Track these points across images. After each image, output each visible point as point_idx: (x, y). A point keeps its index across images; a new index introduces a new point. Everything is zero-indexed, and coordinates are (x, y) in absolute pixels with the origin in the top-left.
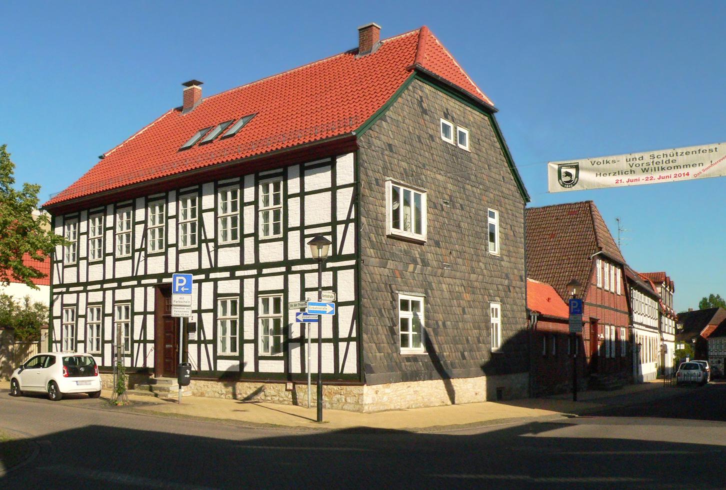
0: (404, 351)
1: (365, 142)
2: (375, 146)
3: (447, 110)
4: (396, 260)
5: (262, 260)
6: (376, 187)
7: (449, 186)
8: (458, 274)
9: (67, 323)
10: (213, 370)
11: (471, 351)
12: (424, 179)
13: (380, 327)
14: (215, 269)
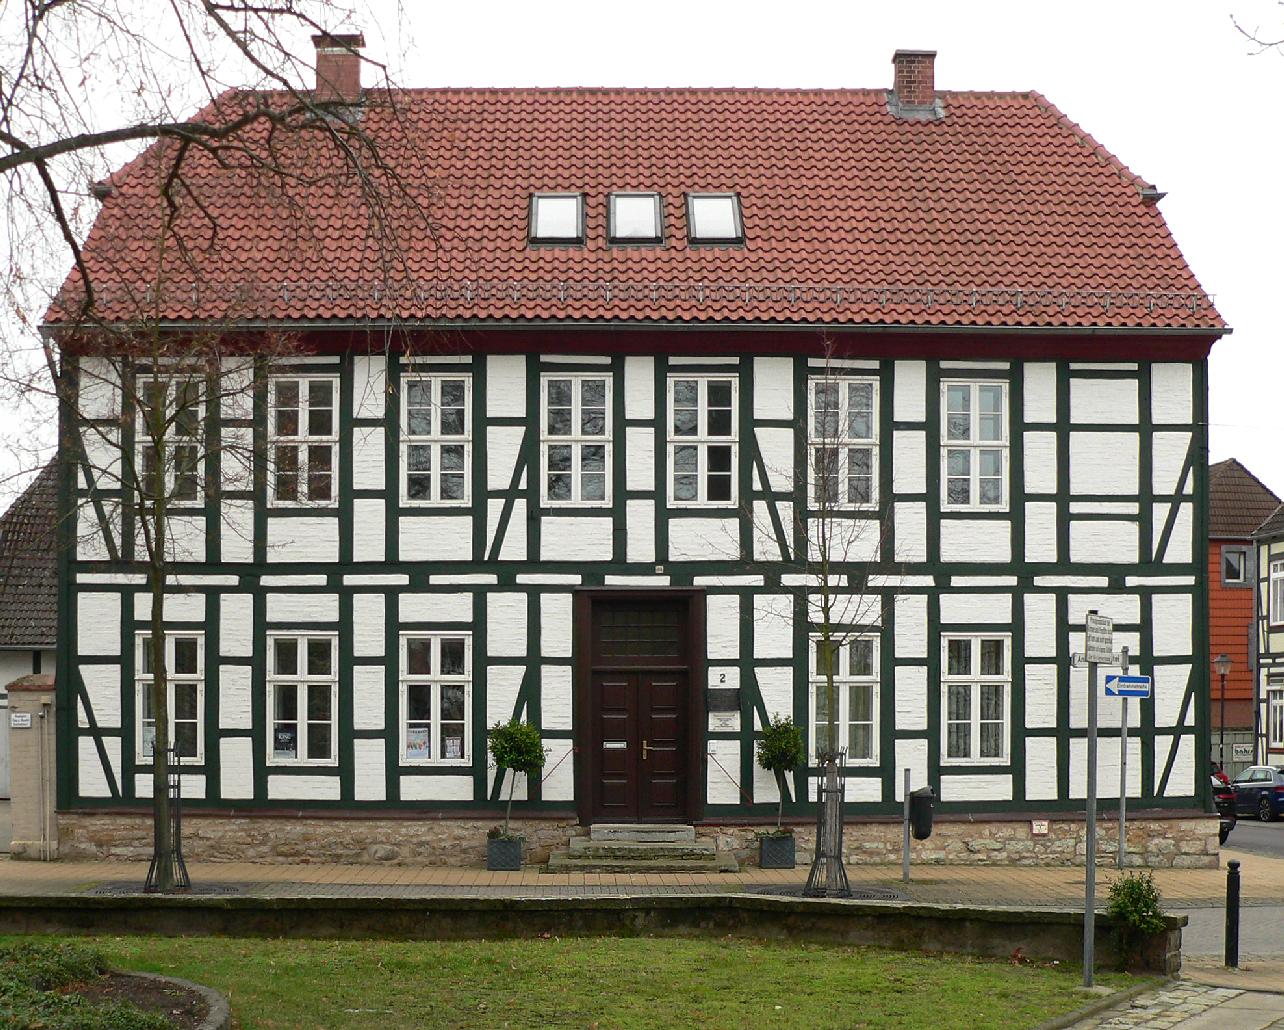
5: (948, 555)
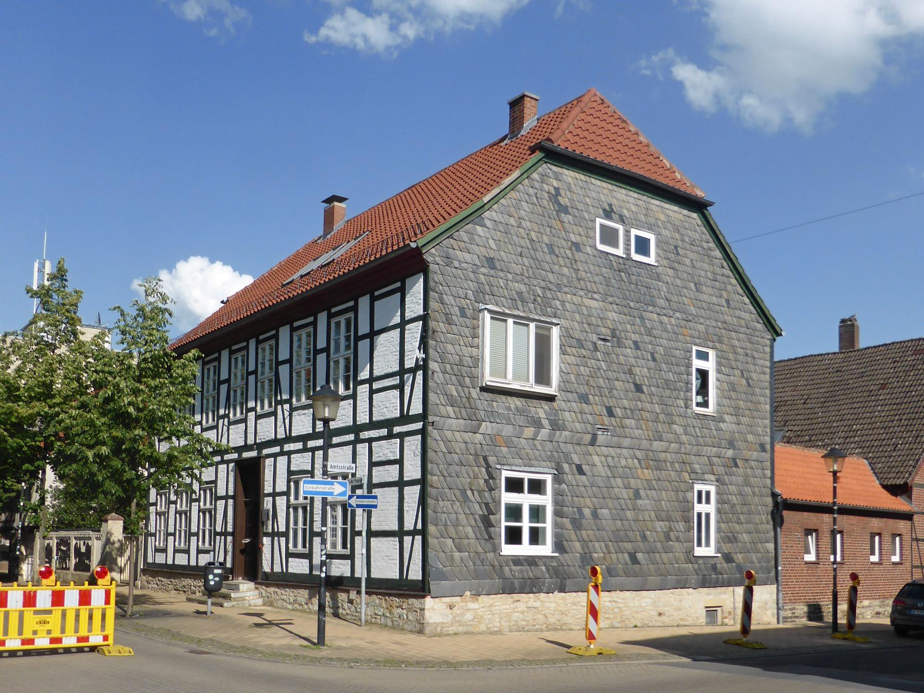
0: (509, 550)
1: (440, 256)
2: (460, 261)
3: (610, 205)
4: (498, 421)
6: (461, 319)
7: (611, 315)
8: (627, 442)
9: (296, 502)
10: (285, 571)
11: (650, 551)
12: (560, 307)
13: (462, 517)
14: (289, 439)
